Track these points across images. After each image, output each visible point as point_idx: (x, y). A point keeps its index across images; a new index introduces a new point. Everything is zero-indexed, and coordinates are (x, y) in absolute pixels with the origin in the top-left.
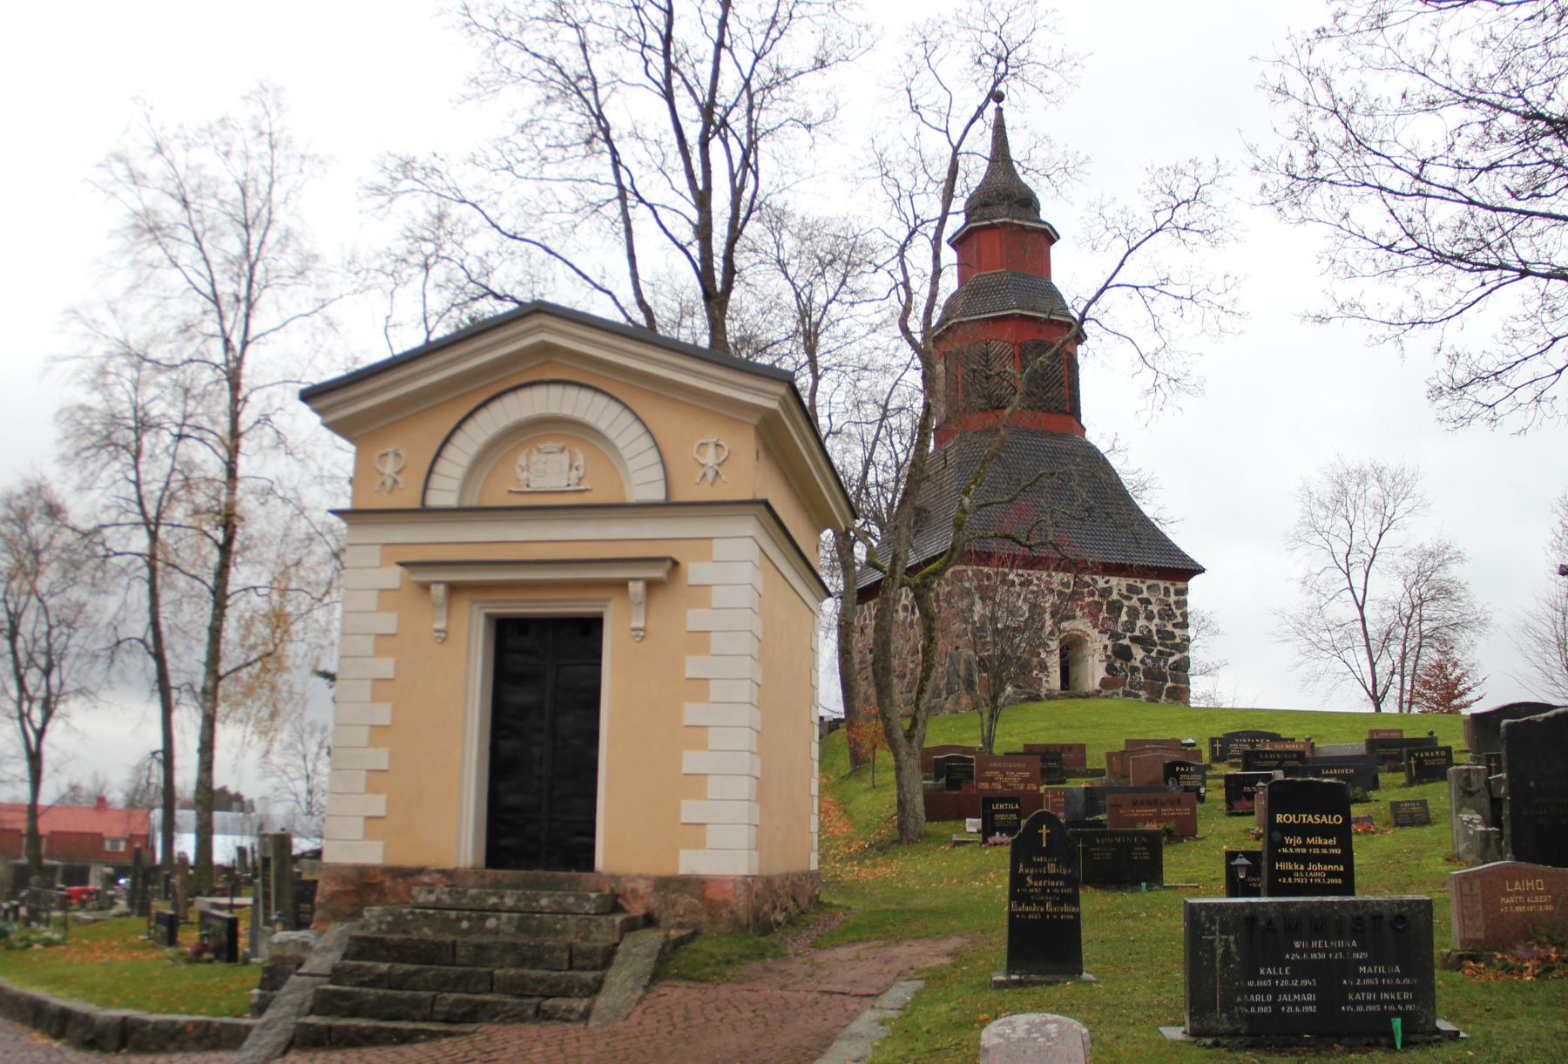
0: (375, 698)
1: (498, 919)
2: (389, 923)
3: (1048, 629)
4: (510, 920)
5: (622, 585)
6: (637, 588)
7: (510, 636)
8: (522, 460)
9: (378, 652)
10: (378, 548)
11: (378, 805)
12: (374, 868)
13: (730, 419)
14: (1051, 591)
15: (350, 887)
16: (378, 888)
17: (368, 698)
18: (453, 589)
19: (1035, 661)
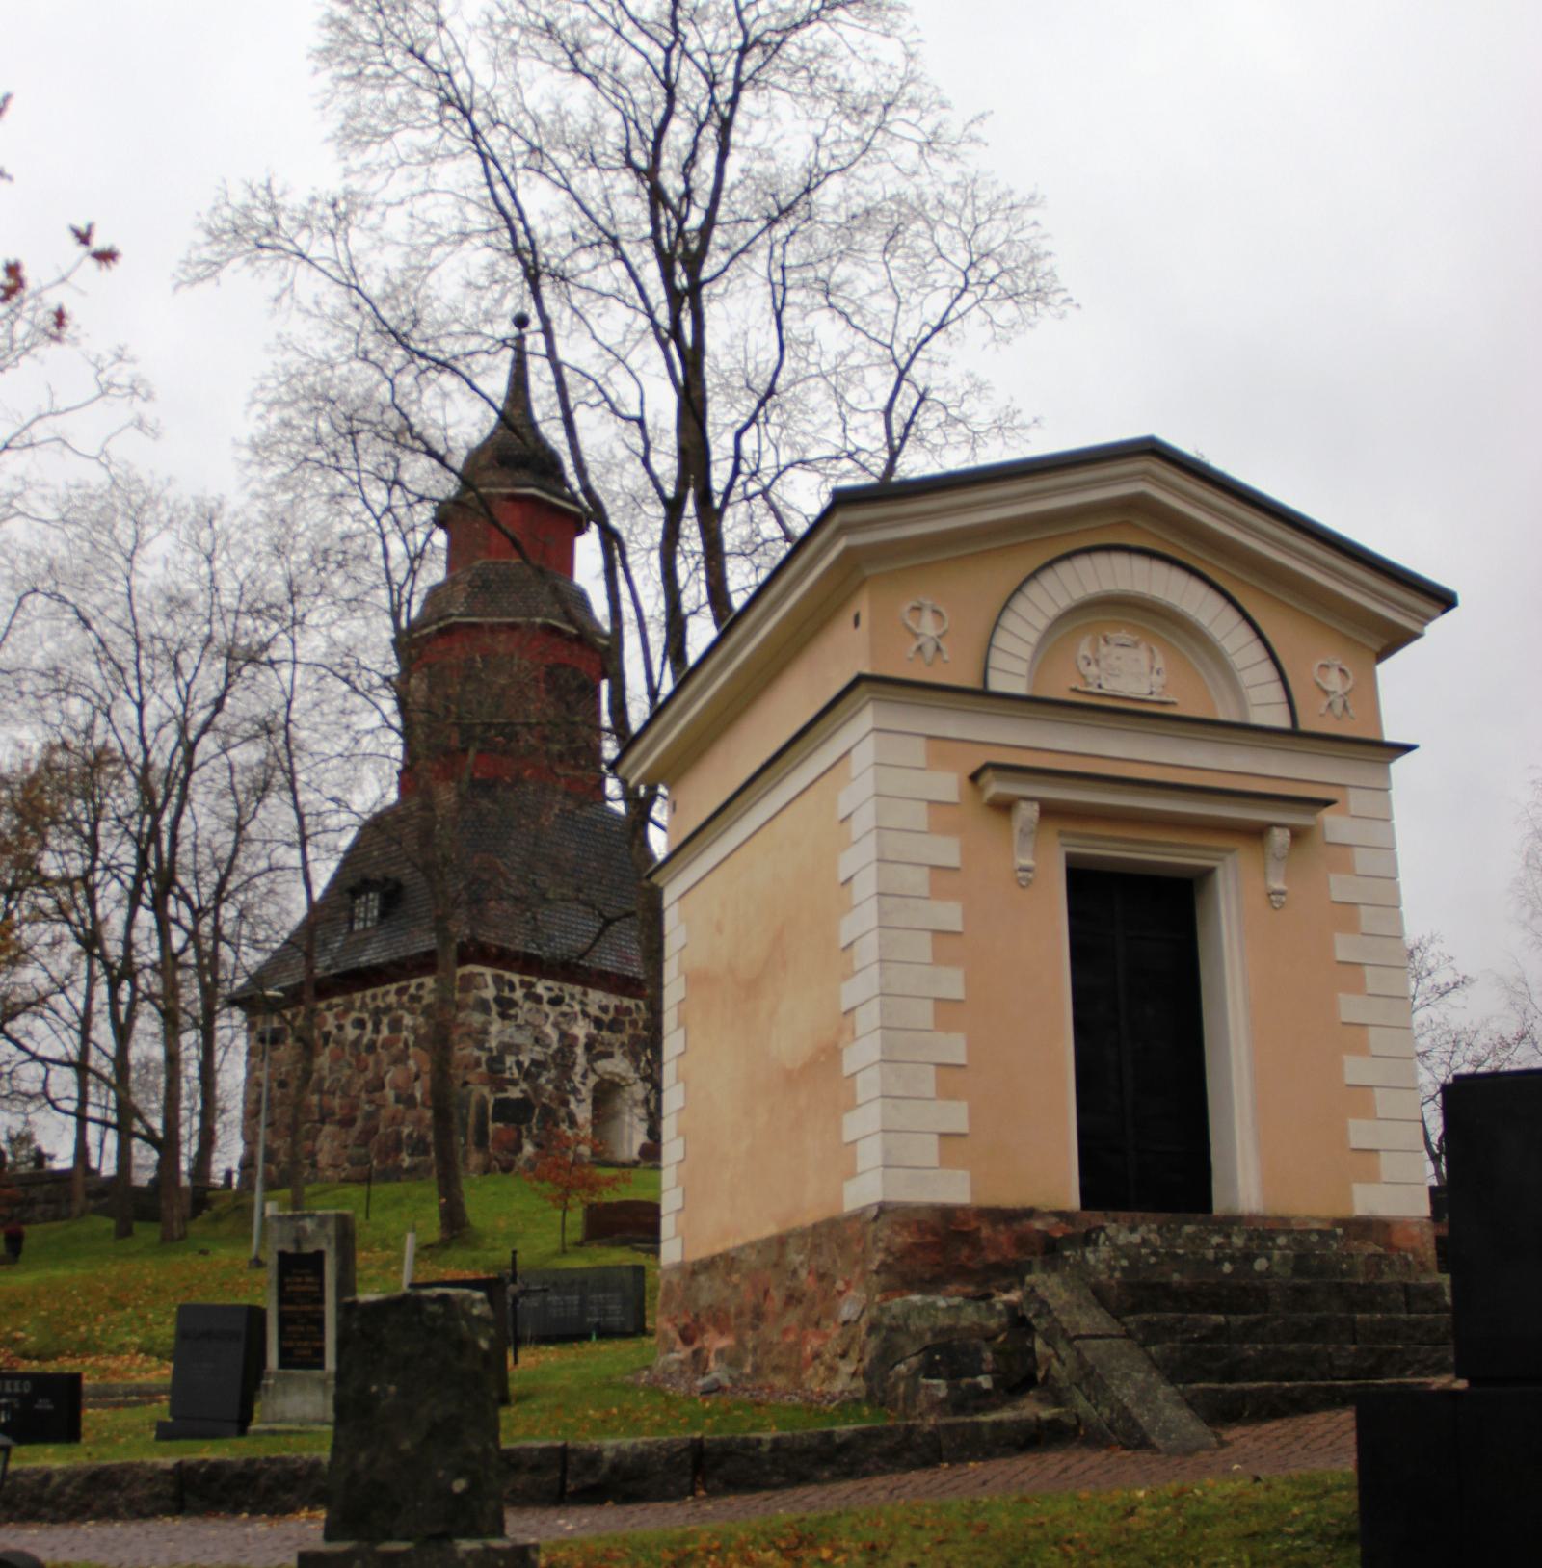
0: (938, 959)
1: (1269, 1259)
2: (1123, 1269)
3: (579, 1069)
4: (1284, 1257)
5: (1257, 833)
6: (1280, 838)
7: (1090, 888)
8: (1085, 649)
9: (937, 893)
10: (921, 742)
11: (956, 1116)
12: (963, 1208)
13: (1348, 639)
14: (585, 1014)
15: (929, 1238)
16: (968, 1238)
17: (928, 958)
18: (1050, 811)
19: (562, 1113)
